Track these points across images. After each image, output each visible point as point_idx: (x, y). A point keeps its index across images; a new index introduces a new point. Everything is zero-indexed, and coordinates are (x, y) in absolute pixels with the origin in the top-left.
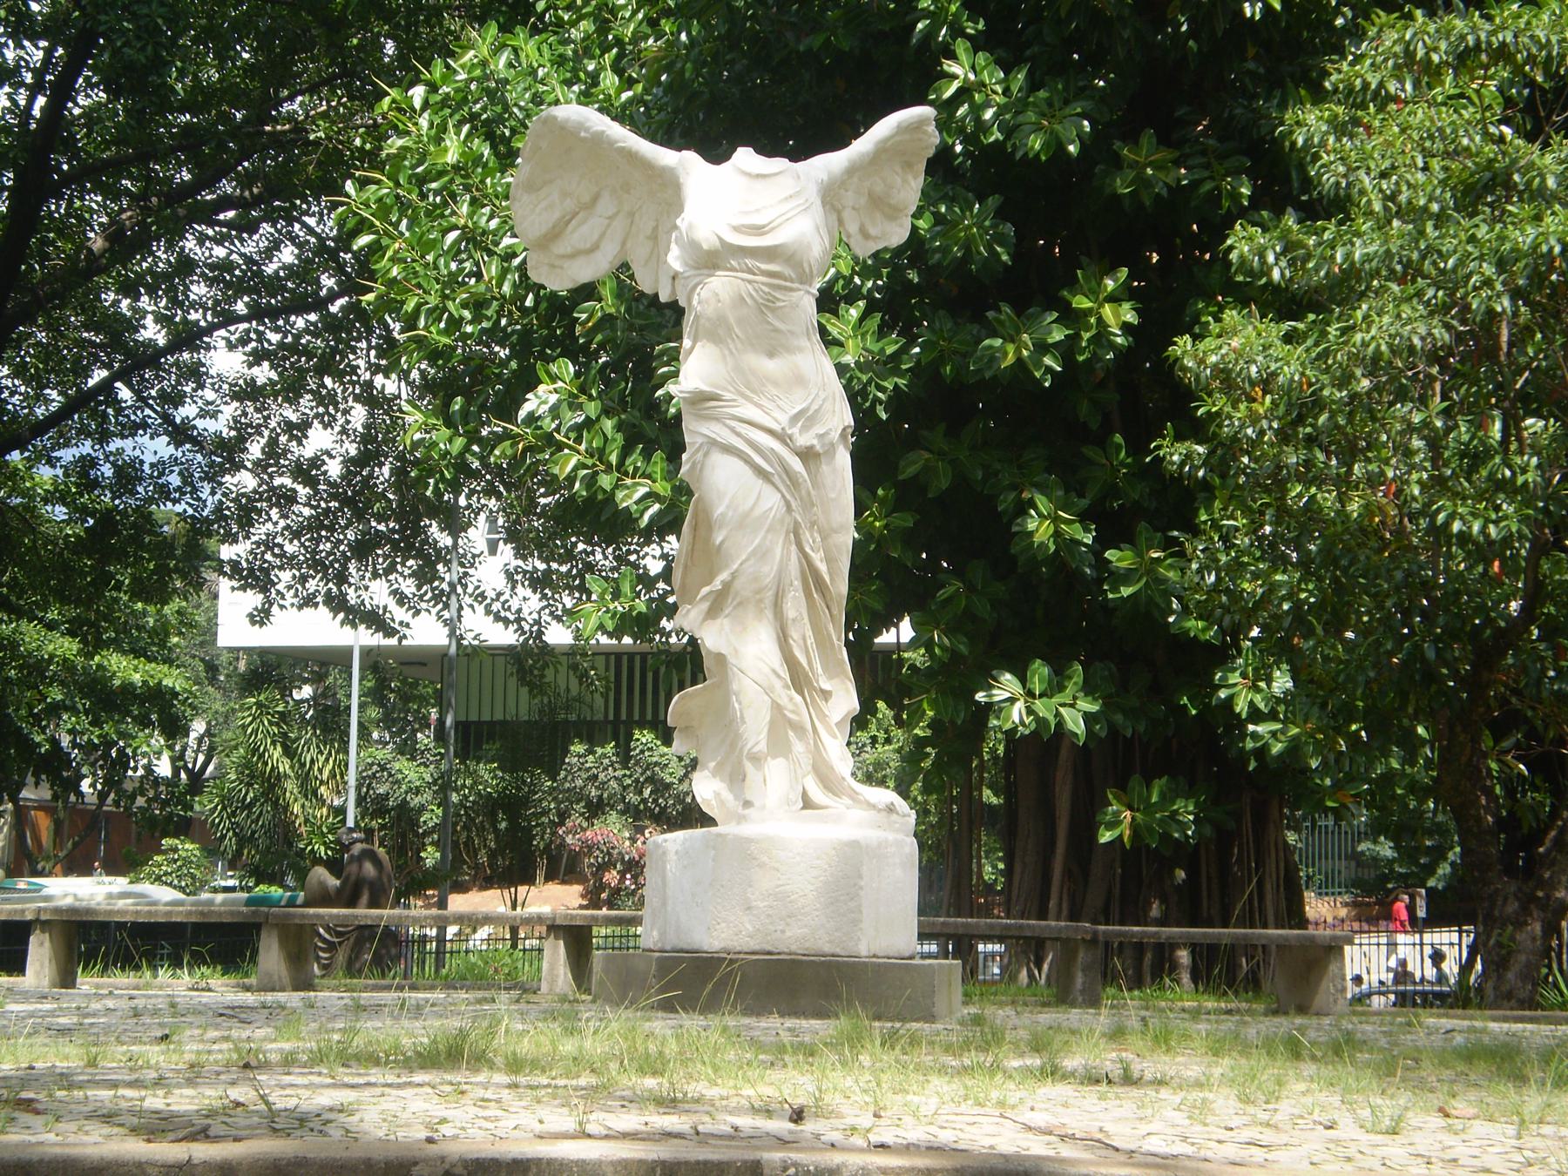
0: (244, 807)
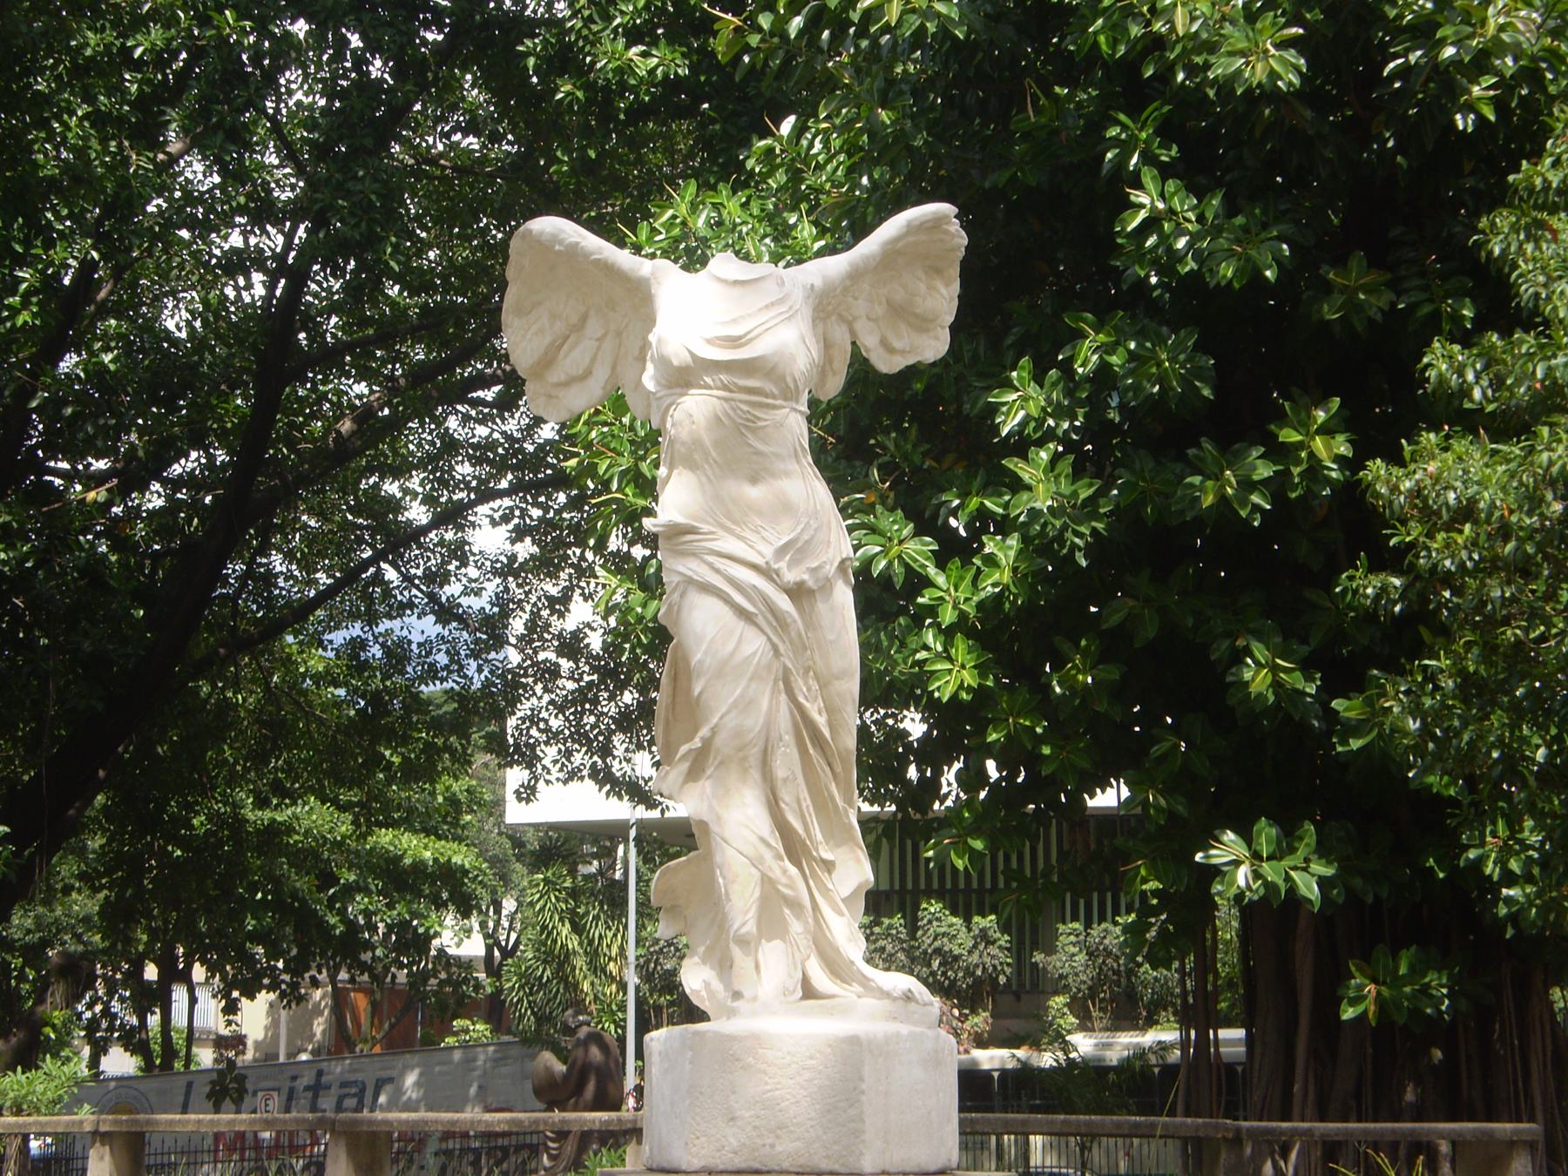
0: (541, 986)
